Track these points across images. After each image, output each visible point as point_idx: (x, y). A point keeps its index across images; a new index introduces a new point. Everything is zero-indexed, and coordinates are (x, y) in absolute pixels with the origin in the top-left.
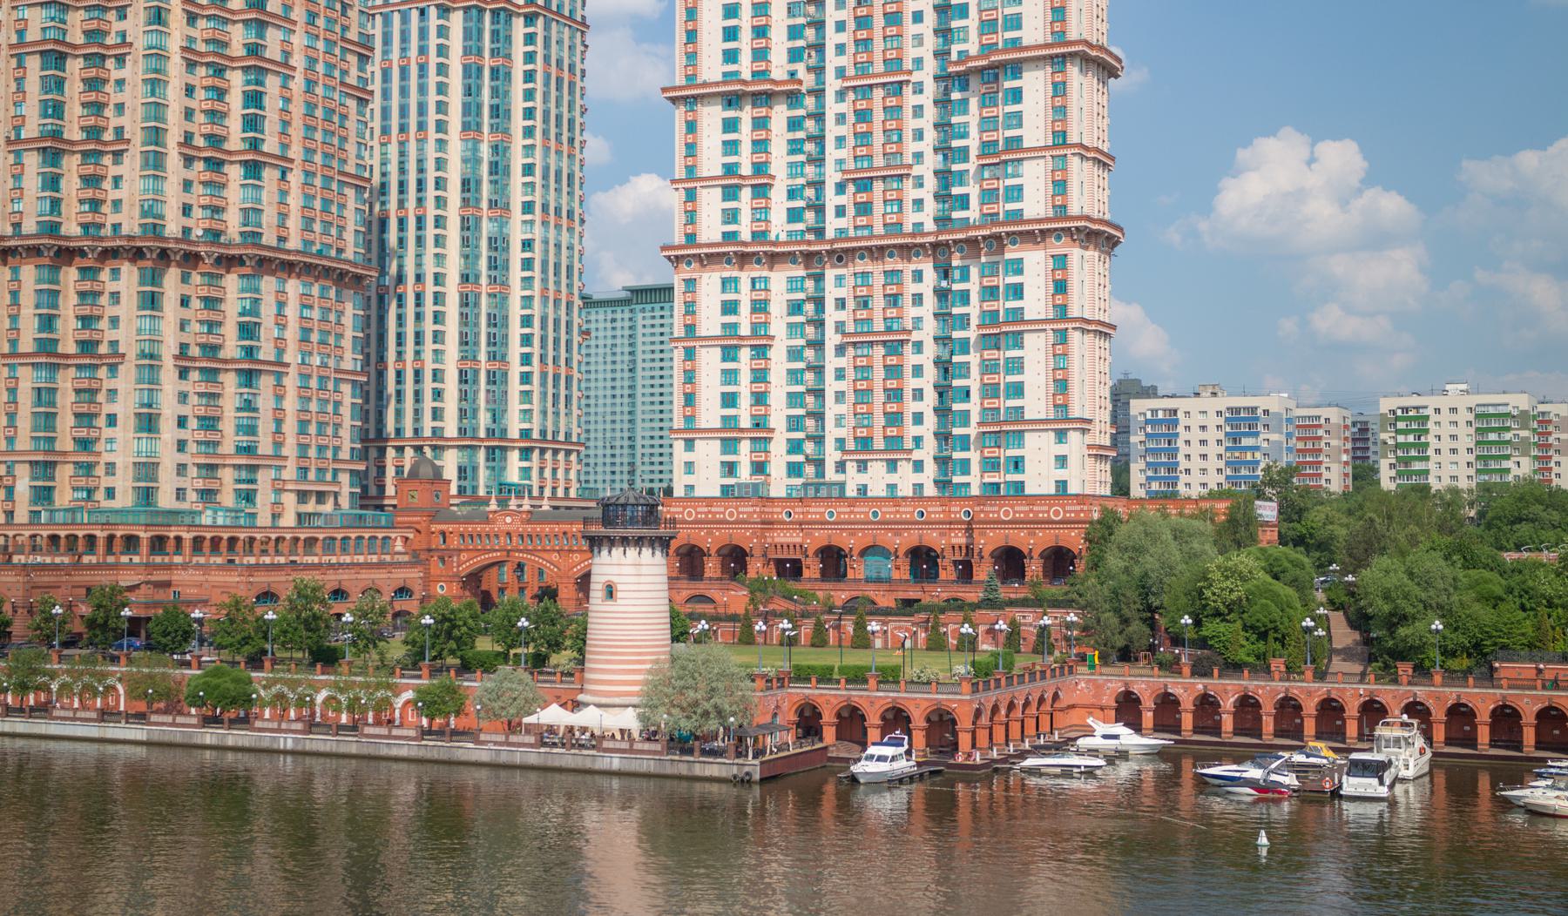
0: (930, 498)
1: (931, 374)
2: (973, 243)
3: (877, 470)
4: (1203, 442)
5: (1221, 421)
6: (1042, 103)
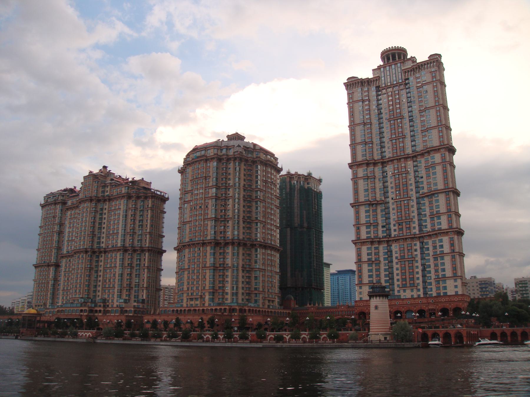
1: (420, 268)
2: (430, 236)
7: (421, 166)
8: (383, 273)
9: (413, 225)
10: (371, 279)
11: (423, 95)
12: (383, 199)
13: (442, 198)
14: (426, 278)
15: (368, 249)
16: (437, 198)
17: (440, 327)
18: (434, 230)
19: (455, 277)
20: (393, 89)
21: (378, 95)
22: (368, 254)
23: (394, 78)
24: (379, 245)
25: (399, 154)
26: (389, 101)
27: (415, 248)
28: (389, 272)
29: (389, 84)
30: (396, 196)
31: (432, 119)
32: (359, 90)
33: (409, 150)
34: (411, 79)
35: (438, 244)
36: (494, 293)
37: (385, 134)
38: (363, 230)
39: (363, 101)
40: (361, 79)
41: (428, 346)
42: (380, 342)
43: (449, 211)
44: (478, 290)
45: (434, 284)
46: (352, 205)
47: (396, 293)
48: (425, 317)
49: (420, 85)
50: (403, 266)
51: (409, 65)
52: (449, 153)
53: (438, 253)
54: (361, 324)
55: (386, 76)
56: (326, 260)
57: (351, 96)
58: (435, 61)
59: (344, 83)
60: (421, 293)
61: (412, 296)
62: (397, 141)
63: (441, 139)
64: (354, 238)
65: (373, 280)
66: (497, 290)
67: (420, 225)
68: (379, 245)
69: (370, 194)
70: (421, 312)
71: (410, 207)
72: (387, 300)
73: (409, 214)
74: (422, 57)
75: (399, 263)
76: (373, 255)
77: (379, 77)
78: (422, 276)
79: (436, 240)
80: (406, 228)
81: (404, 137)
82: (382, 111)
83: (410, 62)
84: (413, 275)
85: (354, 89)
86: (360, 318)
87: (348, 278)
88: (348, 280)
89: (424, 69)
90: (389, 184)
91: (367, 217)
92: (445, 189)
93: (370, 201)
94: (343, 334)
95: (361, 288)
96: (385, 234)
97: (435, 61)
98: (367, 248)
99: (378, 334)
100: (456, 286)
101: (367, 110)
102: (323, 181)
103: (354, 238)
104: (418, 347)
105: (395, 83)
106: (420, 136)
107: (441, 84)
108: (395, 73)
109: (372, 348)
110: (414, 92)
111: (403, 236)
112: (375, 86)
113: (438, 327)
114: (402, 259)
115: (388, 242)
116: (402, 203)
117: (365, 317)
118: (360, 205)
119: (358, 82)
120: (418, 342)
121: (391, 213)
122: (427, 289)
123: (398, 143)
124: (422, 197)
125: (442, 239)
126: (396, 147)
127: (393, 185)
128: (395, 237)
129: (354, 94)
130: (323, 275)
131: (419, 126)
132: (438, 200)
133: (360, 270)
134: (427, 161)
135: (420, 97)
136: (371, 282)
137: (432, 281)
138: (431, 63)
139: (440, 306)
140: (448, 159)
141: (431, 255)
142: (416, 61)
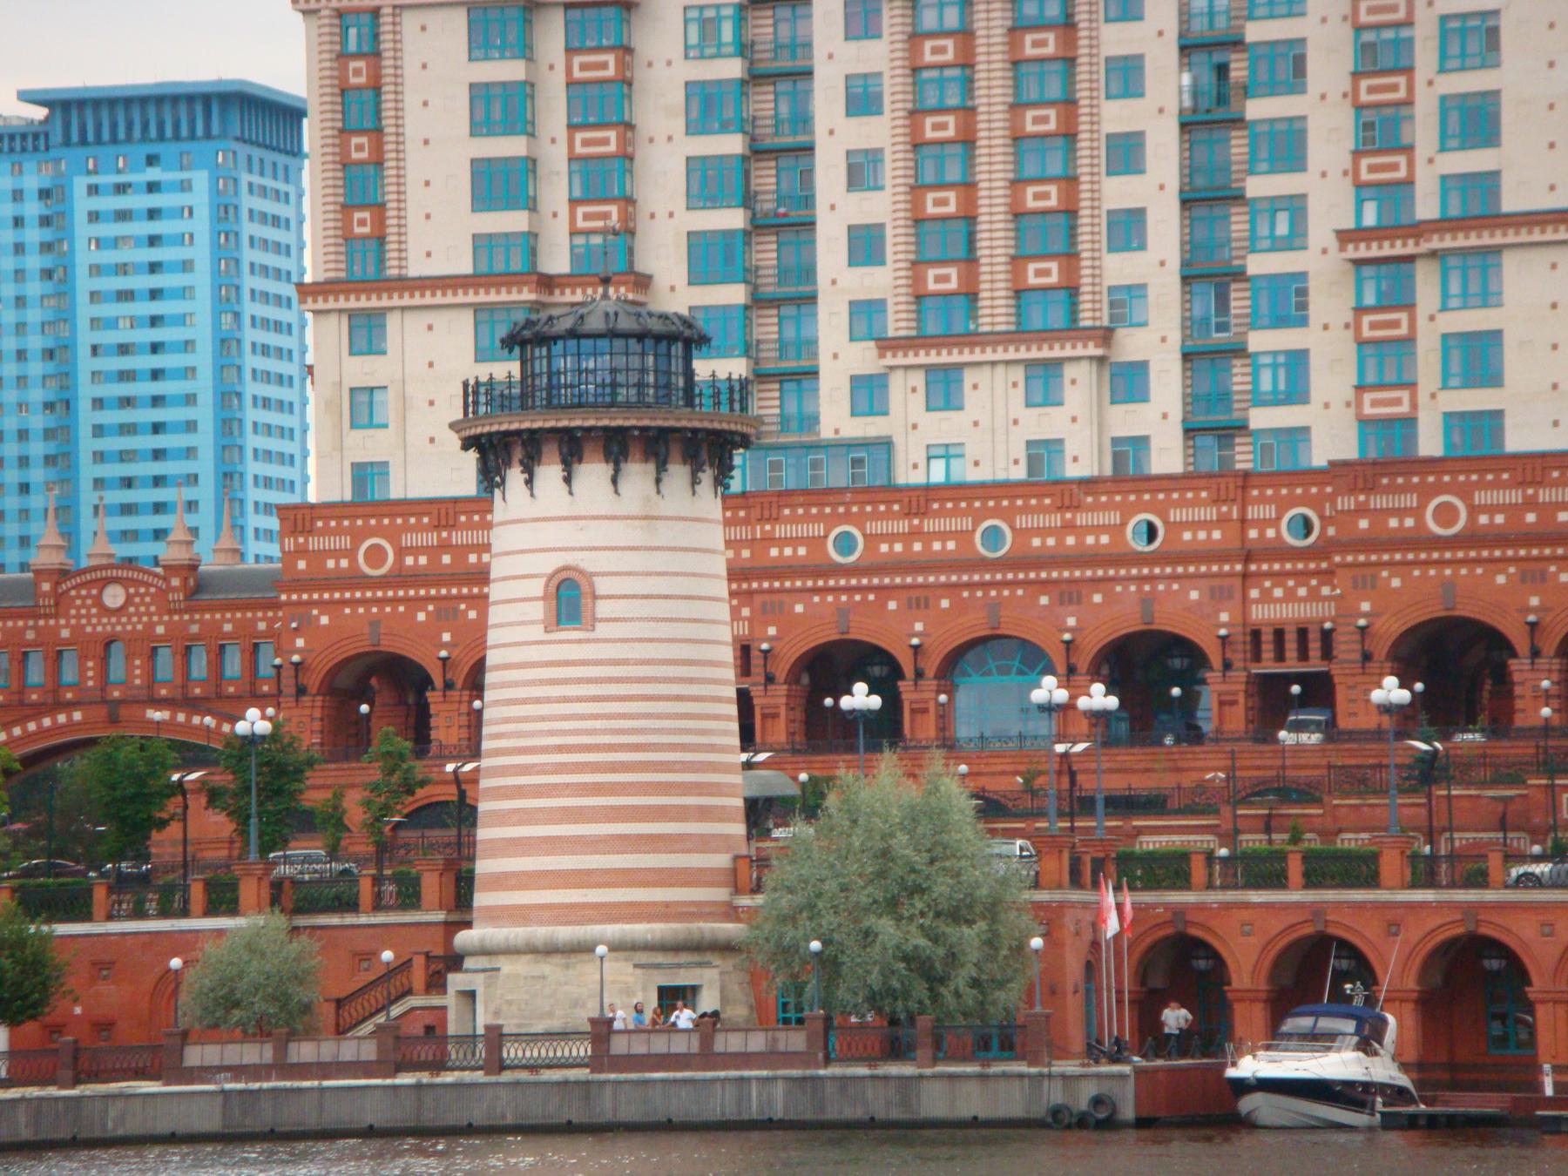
0: (1168, 481)
1: (1169, 85)
8: (668, 152)
10: (514, 221)
14: (1238, 222)
17: (1391, 864)
28: (748, 127)
41: (1218, 1111)
42: (601, 1058)
45: (1331, 301)
47: (836, 417)
48: (1193, 735)
54: (355, 810)
60: (1160, 426)
61: (1042, 452)
65: (531, 241)
70: (1151, 671)
72: (708, 503)
78: (1186, 203)
84: (1070, 182)
86: (348, 737)
87: (200, 196)
88: (201, 226)
94: (106, 961)
95: (366, 333)
99: (583, 949)
104: (1098, 1121)
109: (494, 1131)
113: (1360, 869)
117: (420, 730)
120: (1093, 1051)
122: (1239, 376)
133: (364, 104)
136: (500, 263)
137: (1319, 261)
139: (1398, 598)
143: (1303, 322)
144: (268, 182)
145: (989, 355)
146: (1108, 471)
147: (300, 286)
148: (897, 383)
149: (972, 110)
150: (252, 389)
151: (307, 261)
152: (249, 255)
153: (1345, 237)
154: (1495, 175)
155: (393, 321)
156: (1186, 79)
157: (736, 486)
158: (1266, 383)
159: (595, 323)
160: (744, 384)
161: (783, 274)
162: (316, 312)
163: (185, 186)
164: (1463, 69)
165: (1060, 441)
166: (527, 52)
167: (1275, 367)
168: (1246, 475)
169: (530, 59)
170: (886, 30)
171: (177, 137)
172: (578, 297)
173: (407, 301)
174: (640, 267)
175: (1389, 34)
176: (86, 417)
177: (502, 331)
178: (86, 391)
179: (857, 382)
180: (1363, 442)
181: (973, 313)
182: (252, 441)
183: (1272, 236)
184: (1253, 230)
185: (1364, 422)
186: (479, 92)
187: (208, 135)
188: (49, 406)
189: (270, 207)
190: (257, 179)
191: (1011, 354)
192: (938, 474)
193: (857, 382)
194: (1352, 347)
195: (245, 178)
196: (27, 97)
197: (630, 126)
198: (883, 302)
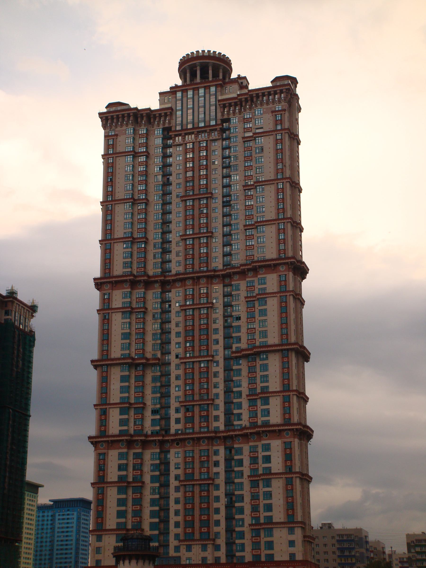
1: (223, 500)
2: (245, 436)
3: (196, 549)
4: (326, 553)
5: (334, 541)
6: (278, 371)
7: (239, 295)
9: (215, 413)
10: (123, 520)
11: (254, 155)
12: (159, 356)
13: (274, 363)
15: (121, 456)
16: (265, 362)
18: (254, 425)
19: (290, 523)
20: (196, 137)
21: (165, 147)
22: (120, 468)
23: (202, 116)
24: (144, 448)
25: (197, 268)
26: (186, 160)
27: (215, 458)
29: (190, 126)
30: (186, 352)
31: (266, 202)
32: (130, 131)
33: (217, 263)
34: (235, 120)
35: (261, 454)
36: (367, 562)
37: (172, 226)
38: (115, 416)
39: (135, 155)
40: (136, 109)
43: (286, 388)
44: (334, 553)
46: (96, 364)
47: (172, 553)
49: (251, 134)
50: (189, 494)
51: (232, 92)
52: (294, 274)
53: (261, 472)
55: (185, 110)
56: (31, 475)
57: (111, 142)
58: (285, 89)
59: (100, 114)
60: (222, 554)
62: (196, 242)
63: (282, 247)
64: (96, 357)
65: (126, 523)
66: (372, 555)
67: (228, 413)
68: (144, 448)
69: (134, 343)
71: (211, 375)
73: (207, 389)
74: (259, 80)
75: (182, 489)
76: (131, 469)
77: (171, 108)
79: (257, 446)
80: (201, 416)
81: (210, 235)
82: (171, 178)
83: (236, 86)
84: (208, 515)
85: (119, 129)
87: (75, 516)
88: (75, 521)
89: (262, 104)
90: (172, 325)
91: (123, 390)
92: (282, 345)
93: (133, 359)
95: (99, 538)
96: (158, 428)
97: (285, 89)
98: (120, 454)
100: (292, 543)
101: (141, 174)
102: (39, 309)
103: (93, 432)
105: (202, 125)
106: (241, 237)
107: (290, 137)
108: (203, 106)
110: (238, 149)
111: (193, 433)
112: (161, 127)
114: (187, 480)
115: (162, 443)
116: (196, 366)
118: (111, 365)
119: (129, 116)
121: (173, 386)
123: (196, 247)
124: (236, 357)
125: (269, 444)
126: (193, 254)
127: (181, 329)
128: (176, 434)
129: (119, 137)
130: (22, 509)
131: (242, 217)
132: (267, 365)
134: (250, 287)
135: (248, 158)
136: (121, 527)
137: (246, 529)
138: (275, 93)
140: (291, 287)
141: (245, 476)
142: (247, 87)
143: (244, 539)
144: (86, 514)
145: (196, 543)
146: (214, 562)
147: (90, 530)
148: (182, 547)
149: (194, 504)
150: (81, 547)
151: (91, 526)
152: (82, 525)
153: (250, 525)
154: (272, 516)
155: (103, 537)
156: (226, 500)
157: (156, 564)
158: (238, 549)
159: (135, 537)
160: (158, 547)
161: (165, 426)
162: (92, 535)
163: (73, 514)
164: (267, 500)
165: (207, 557)
166: (126, 493)
167: (240, 546)
168: (235, 563)
169: (126, 506)
170: (181, 491)
171: (72, 507)
172: (132, 532)
173: (106, 533)
174: (143, 480)
175: (256, 494)
176: (55, 552)
177: (120, 538)
178: (55, 547)
179: (175, 547)
180: (253, 558)
181: (194, 536)
182: (81, 556)
183: (239, 525)
184: (236, 524)
185: (253, 555)
186: (119, 500)
187: (77, 506)
188: (50, 550)
189: (86, 518)
190: (84, 513)
191: (199, 543)
192: (188, 562)
193: (175, 547)
194: (251, 543)
195: (82, 513)
196: (50, 501)
197: (144, 339)
198: (180, 534)
